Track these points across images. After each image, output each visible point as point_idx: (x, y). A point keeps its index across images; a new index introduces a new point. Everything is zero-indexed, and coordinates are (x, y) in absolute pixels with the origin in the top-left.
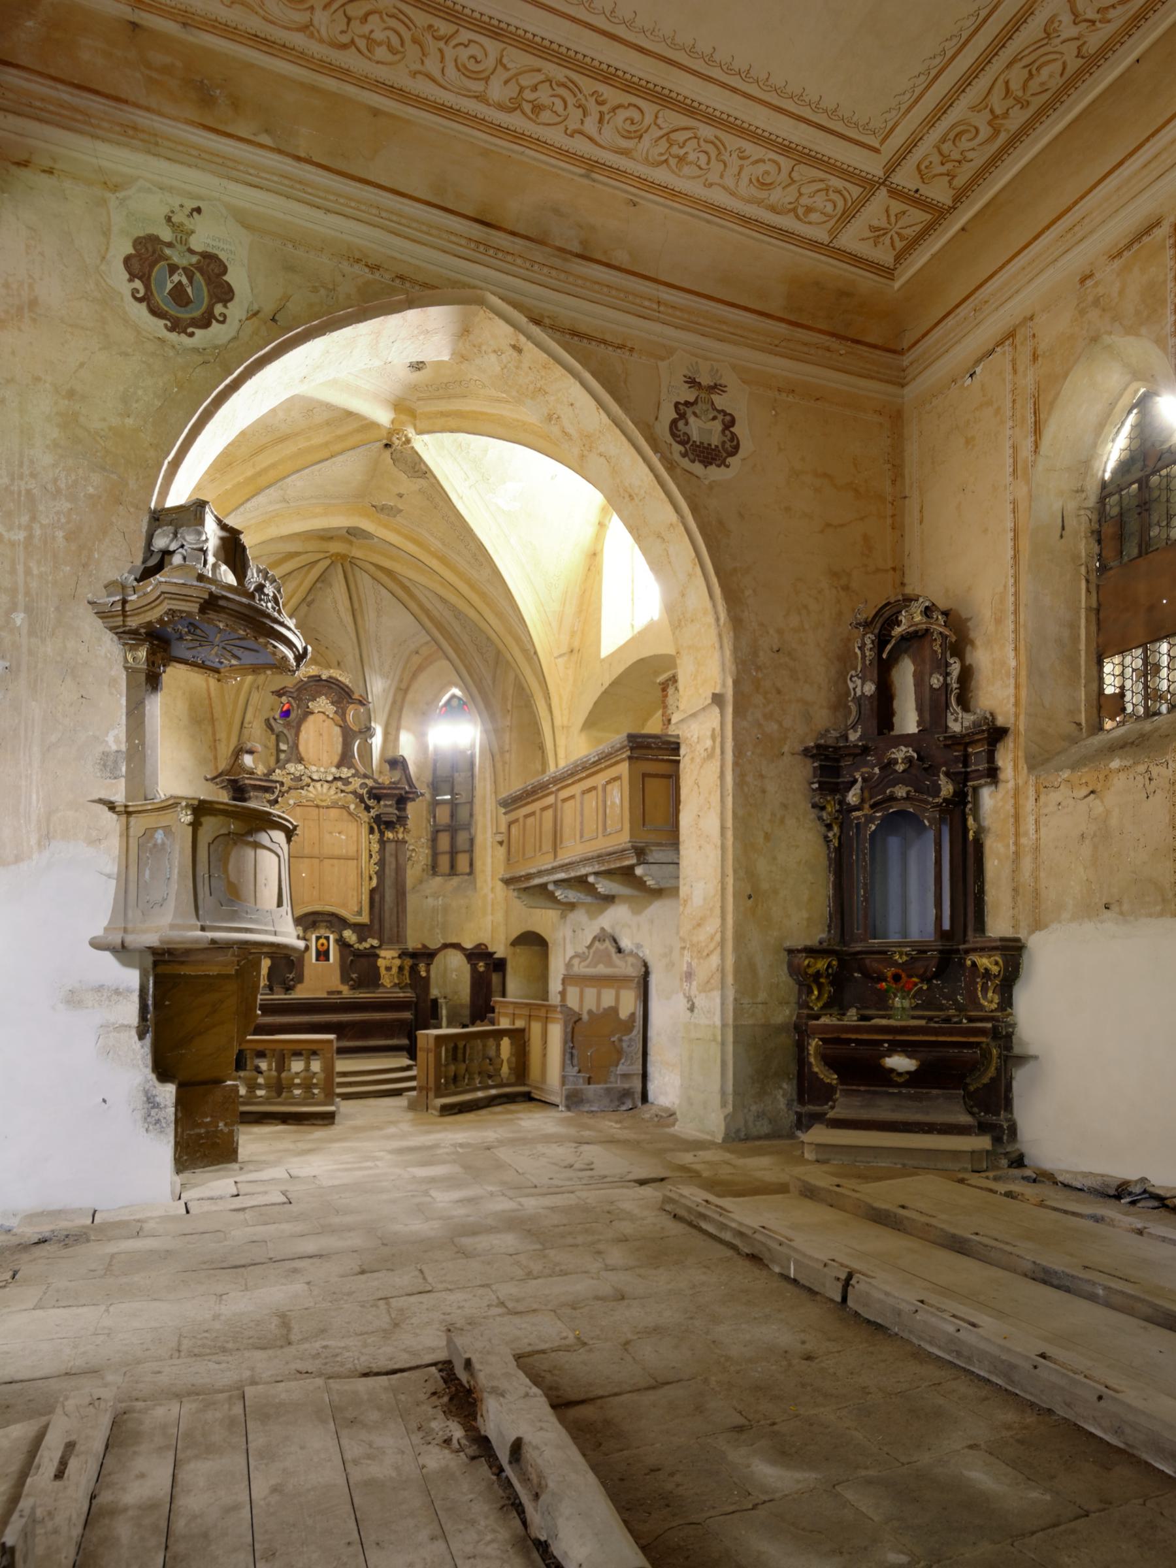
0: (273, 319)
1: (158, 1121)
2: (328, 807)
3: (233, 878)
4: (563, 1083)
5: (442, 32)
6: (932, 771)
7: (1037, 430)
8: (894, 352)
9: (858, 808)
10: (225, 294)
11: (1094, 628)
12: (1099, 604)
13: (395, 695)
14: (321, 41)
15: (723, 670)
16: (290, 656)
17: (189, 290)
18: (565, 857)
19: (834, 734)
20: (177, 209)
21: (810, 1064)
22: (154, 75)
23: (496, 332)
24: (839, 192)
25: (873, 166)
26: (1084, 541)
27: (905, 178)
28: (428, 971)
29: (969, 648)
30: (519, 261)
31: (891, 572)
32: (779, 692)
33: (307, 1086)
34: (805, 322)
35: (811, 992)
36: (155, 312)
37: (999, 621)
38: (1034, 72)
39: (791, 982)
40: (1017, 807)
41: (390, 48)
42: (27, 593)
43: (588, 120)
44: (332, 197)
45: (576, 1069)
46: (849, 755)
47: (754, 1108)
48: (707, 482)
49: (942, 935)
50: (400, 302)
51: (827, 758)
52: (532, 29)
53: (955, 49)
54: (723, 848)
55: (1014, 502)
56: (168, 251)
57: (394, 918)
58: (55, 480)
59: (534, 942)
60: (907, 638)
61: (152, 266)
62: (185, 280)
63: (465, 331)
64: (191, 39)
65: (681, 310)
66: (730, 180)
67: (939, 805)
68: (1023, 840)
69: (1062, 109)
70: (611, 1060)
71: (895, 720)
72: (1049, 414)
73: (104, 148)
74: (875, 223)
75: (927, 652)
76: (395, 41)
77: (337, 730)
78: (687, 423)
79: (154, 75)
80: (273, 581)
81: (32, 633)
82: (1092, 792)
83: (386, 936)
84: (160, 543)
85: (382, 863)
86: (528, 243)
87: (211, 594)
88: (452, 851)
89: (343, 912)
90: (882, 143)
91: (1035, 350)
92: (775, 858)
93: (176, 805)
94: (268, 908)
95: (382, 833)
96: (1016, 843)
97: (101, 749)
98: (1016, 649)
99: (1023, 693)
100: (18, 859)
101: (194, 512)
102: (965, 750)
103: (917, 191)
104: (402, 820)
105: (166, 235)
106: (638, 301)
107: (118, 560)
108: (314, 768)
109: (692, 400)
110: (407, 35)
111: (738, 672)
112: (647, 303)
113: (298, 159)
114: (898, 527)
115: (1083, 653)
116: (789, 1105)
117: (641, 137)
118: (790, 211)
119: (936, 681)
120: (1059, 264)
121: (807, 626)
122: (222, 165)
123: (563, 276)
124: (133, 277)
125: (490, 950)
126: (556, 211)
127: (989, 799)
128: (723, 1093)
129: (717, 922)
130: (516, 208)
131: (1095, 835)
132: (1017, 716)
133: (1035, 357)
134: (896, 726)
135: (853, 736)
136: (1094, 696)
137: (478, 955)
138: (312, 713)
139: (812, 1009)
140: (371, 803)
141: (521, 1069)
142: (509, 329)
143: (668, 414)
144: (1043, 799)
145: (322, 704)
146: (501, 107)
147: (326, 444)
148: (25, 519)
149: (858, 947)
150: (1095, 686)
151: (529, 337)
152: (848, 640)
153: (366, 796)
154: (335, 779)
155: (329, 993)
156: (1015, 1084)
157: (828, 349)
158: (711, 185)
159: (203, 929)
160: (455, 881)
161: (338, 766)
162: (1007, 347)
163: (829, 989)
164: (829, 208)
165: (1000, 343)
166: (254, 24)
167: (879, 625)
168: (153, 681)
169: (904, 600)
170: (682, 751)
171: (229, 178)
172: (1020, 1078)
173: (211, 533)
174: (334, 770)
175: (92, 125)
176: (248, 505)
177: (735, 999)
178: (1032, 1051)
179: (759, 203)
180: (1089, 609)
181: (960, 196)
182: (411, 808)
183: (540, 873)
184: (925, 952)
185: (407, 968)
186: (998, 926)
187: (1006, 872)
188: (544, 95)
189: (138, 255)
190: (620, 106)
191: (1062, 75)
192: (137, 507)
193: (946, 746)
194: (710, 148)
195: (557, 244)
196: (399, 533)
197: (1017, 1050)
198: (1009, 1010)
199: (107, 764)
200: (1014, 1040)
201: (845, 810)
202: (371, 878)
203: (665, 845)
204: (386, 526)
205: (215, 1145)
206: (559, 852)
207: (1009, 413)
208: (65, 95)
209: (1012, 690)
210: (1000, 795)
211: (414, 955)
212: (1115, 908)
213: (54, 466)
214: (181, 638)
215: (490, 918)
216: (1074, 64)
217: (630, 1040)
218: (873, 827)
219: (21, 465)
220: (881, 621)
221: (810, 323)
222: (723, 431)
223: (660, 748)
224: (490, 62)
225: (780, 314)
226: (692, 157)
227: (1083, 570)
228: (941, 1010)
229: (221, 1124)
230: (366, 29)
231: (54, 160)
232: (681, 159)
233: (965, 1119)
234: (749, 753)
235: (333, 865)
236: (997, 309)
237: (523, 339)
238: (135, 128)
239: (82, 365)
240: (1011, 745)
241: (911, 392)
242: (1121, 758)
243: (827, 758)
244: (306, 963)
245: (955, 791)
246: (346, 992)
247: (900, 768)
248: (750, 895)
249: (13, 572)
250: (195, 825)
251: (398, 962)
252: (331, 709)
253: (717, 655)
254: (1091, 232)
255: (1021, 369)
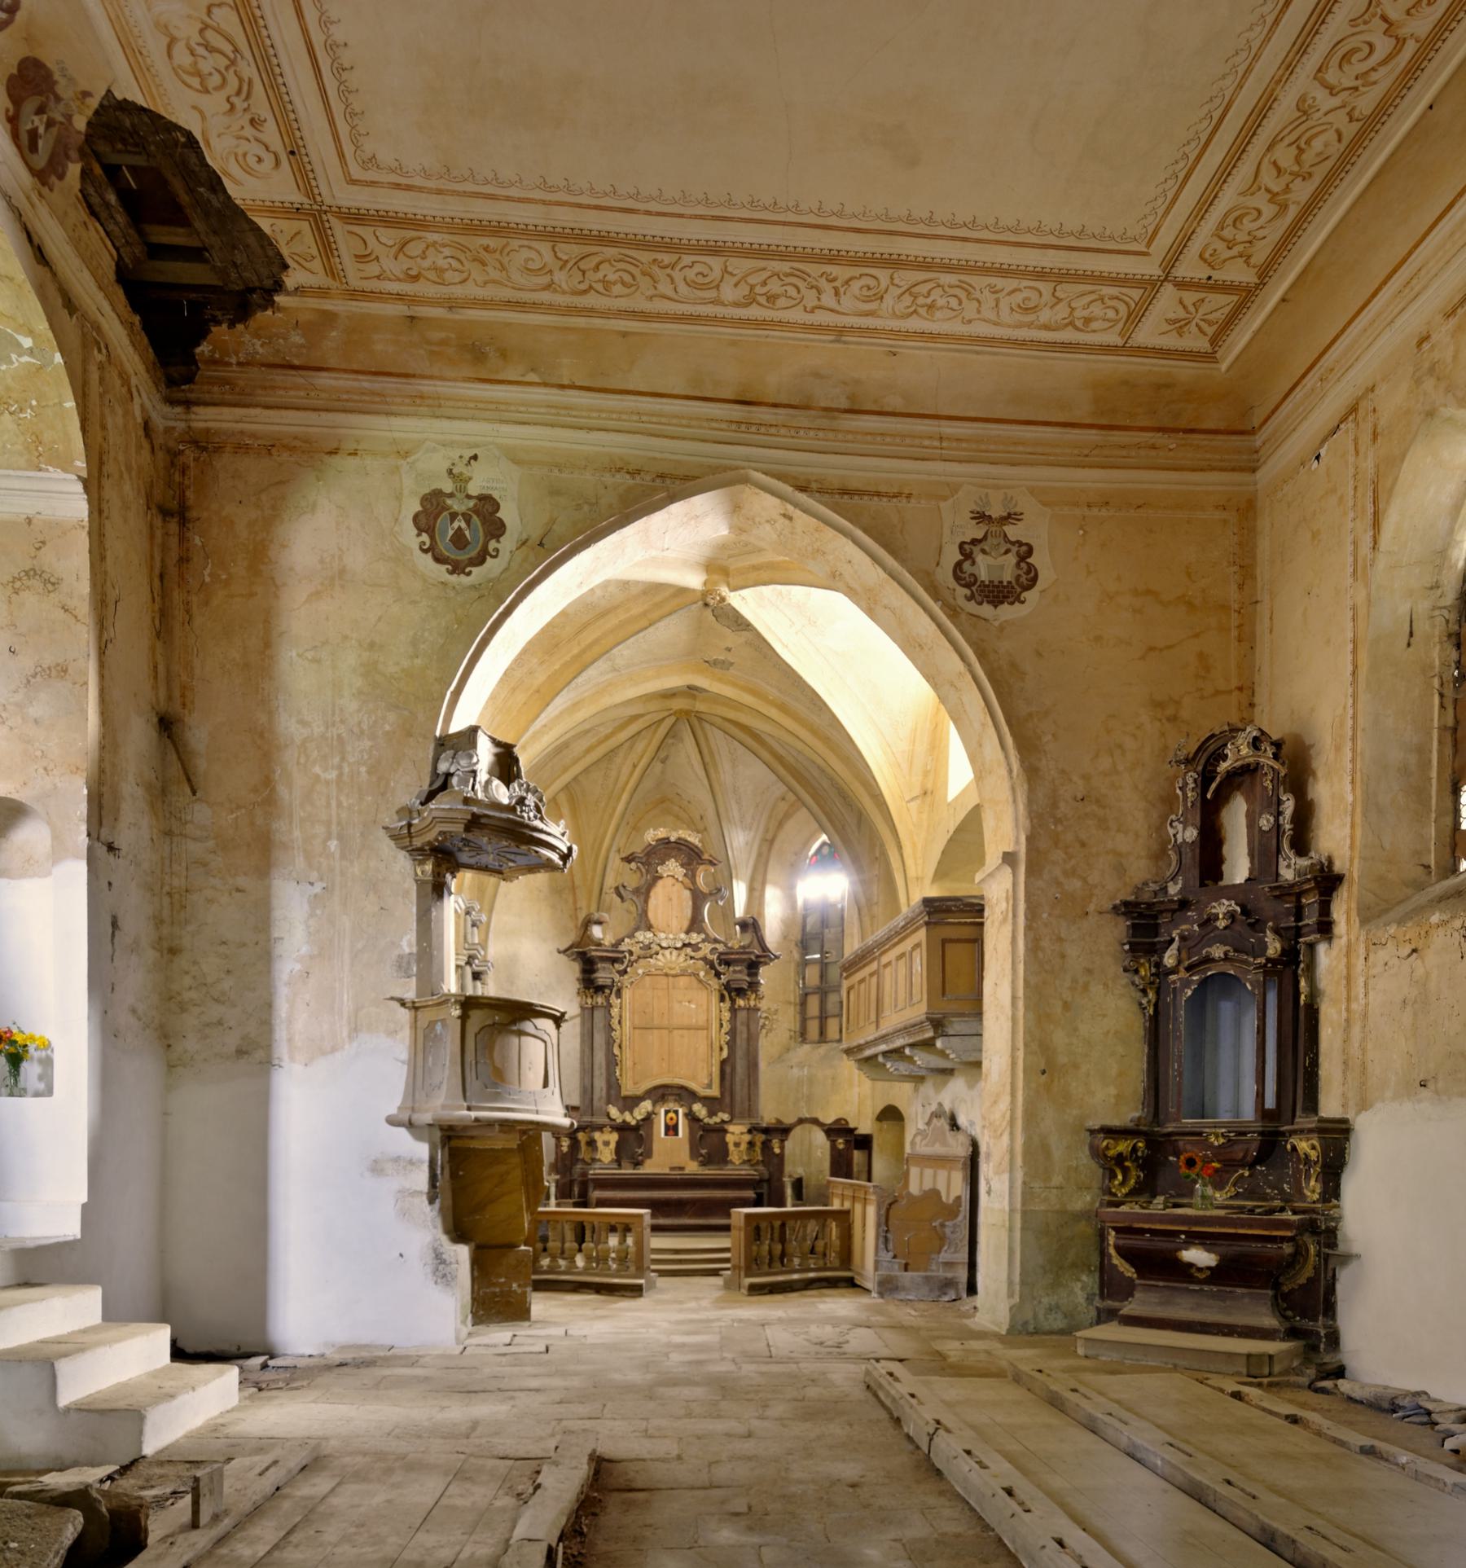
0: (541, 544)
1: (444, 1276)
2: (675, 976)
3: (498, 1063)
4: (876, 1269)
5: (666, 262)
6: (1257, 926)
7: (1376, 524)
8: (1242, 433)
9: (1174, 971)
10: (496, 529)
11: (1449, 750)
12: (1457, 722)
13: (760, 847)
14: (564, 293)
15: (1017, 826)
16: (555, 857)
17: (467, 533)
18: (887, 1026)
19: (1153, 887)
20: (457, 460)
21: (1110, 1256)
22: (436, 349)
23: (765, 505)
24: (1117, 298)
25: (1150, 268)
26: (1438, 647)
27: (1189, 268)
28: (782, 1148)
29: (1311, 779)
30: (783, 431)
31: (1236, 693)
32: (1083, 845)
33: (623, 1259)
34: (1122, 423)
35: (1113, 1176)
36: (439, 559)
37: (1338, 749)
38: (1303, 146)
39: (1093, 1165)
40: (1349, 966)
41: (624, 283)
42: (339, 823)
43: (823, 297)
44: (595, 415)
45: (891, 1254)
46: (1167, 911)
47: (1045, 1300)
48: (996, 624)
49: (1264, 1114)
50: (661, 499)
51: (1141, 915)
52: (747, 240)
53: (1197, 152)
54: (1014, 1019)
55: (1354, 608)
56: (449, 502)
57: (745, 1090)
58: (360, 723)
59: (891, 1115)
60: (1232, 775)
61: (436, 519)
62: (463, 525)
63: (735, 508)
64: (457, 317)
65: (967, 441)
66: (993, 312)
67: (1260, 966)
68: (1354, 1006)
69: (1354, 171)
70: (934, 1244)
71: (1224, 867)
72: (1388, 502)
73: (396, 422)
74: (1172, 316)
75: (1258, 789)
76: (627, 278)
77: (687, 893)
78: (974, 563)
79: (436, 349)
80: (535, 792)
81: (343, 857)
82: (1414, 951)
83: (737, 1110)
84: (443, 767)
85: (732, 1033)
86: (791, 411)
87: (473, 814)
88: (819, 1012)
89: (693, 1085)
90: (1149, 244)
91: (1375, 426)
92: (1076, 1029)
93: (446, 1001)
94: (532, 1089)
95: (733, 1001)
96: (1348, 1010)
97: (396, 952)
98: (1352, 782)
99: (1358, 833)
100: (334, 1050)
101: (469, 736)
102: (1298, 901)
103: (1209, 278)
104: (754, 986)
105: (448, 486)
106: (917, 442)
107: (408, 786)
108: (663, 935)
109: (980, 536)
110: (636, 272)
111: (1033, 827)
112: (927, 442)
113: (562, 387)
114: (1247, 638)
115: (1434, 782)
116: (1089, 1299)
117: (882, 298)
118: (1066, 325)
119: (1266, 822)
120: (1398, 323)
121: (1120, 768)
122: (497, 410)
123: (831, 435)
124: (420, 531)
125: (852, 1125)
126: (817, 375)
127: (1327, 958)
128: (1010, 1283)
129: (1007, 1099)
130: (774, 383)
131: (1415, 1002)
132: (1352, 860)
133: (1375, 436)
134: (1225, 876)
135: (1173, 889)
136: (1448, 831)
137: (838, 1130)
138: (661, 877)
139: (1115, 1195)
140: (721, 969)
141: (846, 1256)
142: (776, 501)
143: (952, 555)
144: (1372, 957)
145: (672, 868)
146: (737, 304)
147: (644, 614)
148: (337, 760)
149: (1170, 1128)
150: (1449, 821)
151: (796, 505)
152: (1172, 781)
153: (716, 963)
154: (685, 945)
155: (672, 1169)
156: (1339, 1287)
157: (1153, 447)
158: (970, 322)
159: (469, 1109)
160: (824, 1048)
161: (687, 932)
162: (1349, 425)
163: (1135, 1175)
164: (1111, 314)
165: (1343, 420)
166: (507, 294)
167: (1203, 761)
168: (439, 889)
169: (1231, 731)
170: (986, 914)
171: (502, 422)
172: (1345, 1280)
173: (485, 753)
174: (683, 936)
175: (387, 403)
176: (580, 680)
177: (1024, 1183)
178: (1356, 1248)
179: (1029, 325)
180: (1443, 728)
181: (1265, 273)
182: (765, 975)
183: (868, 1044)
184: (1244, 1134)
185: (759, 1144)
186: (1330, 1106)
187: (1338, 1043)
188: (775, 287)
189: (425, 511)
190: (851, 279)
191: (1340, 141)
192: (425, 737)
193: (1276, 897)
194: (957, 291)
195: (823, 405)
196: (734, 685)
197: (1342, 1248)
198: (1335, 1202)
199: (402, 965)
200: (1339, 1237)
201: (1161, 972)
202: (721, 1049)
203: (969, 1015)
204: (720, 680)
205: (508, 1303)
206: (881, 1021)
207: (1351, 503)
208: (366, 383)
209: (1348, 830)
210: (1334, 952)
211: (766, 1131)
212: (1431, 1085)
213: (359, 711)
214: (460, 850)
215: (856, 1090)
216: (1350, 130)
217: (955, 1226)
218: (1190, 993)
219: (333, 714)
220: (1206, 755)
221: (1128, 422)
222: (1018, 565)
223: (962, 911)
224: (717, 274)
225: (1088, 421)
226: (941, 302)
227: (1436, 682)
228: (1265, 1199)
229: (515, 1285)
230: (600, 275)
231: (358, 442)
232: (931, 307)
233: (1270, 1321)
234: (1045, 915)
235: (682, 1036)
236: (1339, 380)
237: (790, 508)
238: (422, 397)
239: (380, 619)
240: (1345, 894)
241: (1264, 475)
242: (1441, 911)
243: (1141, 915)
244: (655, 1138)
245: (1283, 949)
246: (693, 1168)
247: (1221, 924)
248: (1044, 1068)
249: (328, 805)
250: (464, 1018)
251: (747, 1138)
252: (680, 872)
253: (1010, 810)
254: (1425, 288)
255: (1362, 450)
